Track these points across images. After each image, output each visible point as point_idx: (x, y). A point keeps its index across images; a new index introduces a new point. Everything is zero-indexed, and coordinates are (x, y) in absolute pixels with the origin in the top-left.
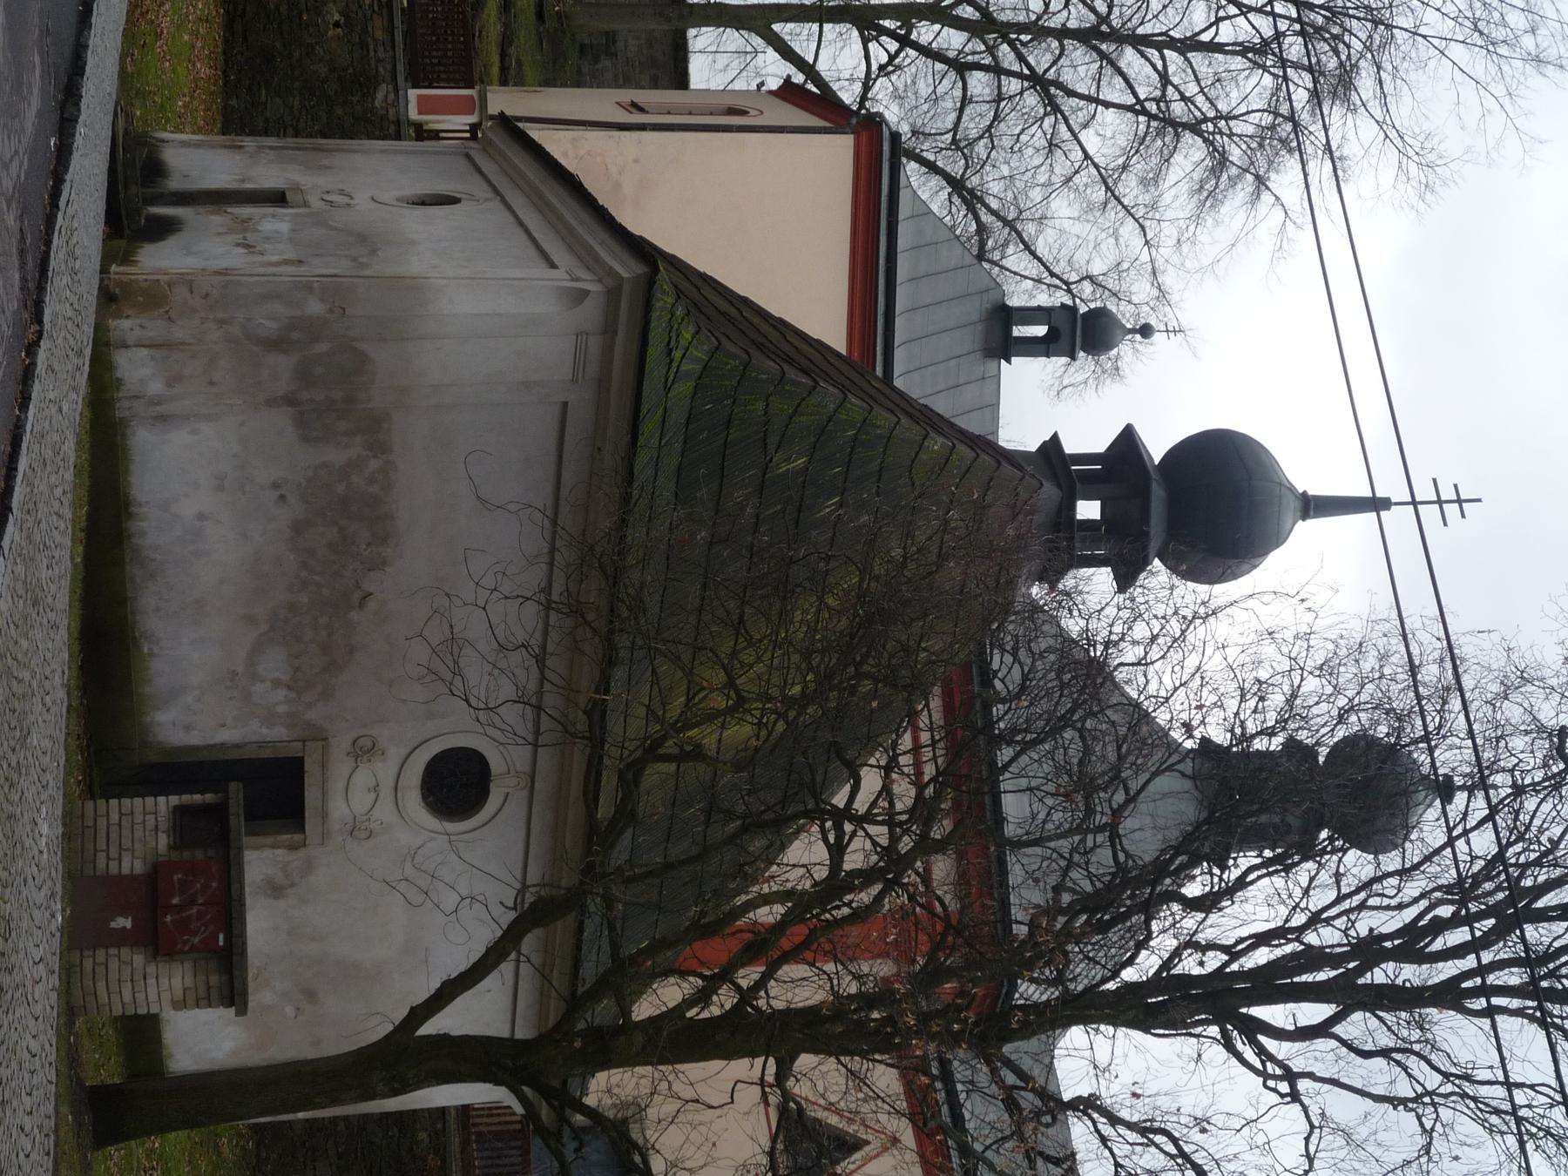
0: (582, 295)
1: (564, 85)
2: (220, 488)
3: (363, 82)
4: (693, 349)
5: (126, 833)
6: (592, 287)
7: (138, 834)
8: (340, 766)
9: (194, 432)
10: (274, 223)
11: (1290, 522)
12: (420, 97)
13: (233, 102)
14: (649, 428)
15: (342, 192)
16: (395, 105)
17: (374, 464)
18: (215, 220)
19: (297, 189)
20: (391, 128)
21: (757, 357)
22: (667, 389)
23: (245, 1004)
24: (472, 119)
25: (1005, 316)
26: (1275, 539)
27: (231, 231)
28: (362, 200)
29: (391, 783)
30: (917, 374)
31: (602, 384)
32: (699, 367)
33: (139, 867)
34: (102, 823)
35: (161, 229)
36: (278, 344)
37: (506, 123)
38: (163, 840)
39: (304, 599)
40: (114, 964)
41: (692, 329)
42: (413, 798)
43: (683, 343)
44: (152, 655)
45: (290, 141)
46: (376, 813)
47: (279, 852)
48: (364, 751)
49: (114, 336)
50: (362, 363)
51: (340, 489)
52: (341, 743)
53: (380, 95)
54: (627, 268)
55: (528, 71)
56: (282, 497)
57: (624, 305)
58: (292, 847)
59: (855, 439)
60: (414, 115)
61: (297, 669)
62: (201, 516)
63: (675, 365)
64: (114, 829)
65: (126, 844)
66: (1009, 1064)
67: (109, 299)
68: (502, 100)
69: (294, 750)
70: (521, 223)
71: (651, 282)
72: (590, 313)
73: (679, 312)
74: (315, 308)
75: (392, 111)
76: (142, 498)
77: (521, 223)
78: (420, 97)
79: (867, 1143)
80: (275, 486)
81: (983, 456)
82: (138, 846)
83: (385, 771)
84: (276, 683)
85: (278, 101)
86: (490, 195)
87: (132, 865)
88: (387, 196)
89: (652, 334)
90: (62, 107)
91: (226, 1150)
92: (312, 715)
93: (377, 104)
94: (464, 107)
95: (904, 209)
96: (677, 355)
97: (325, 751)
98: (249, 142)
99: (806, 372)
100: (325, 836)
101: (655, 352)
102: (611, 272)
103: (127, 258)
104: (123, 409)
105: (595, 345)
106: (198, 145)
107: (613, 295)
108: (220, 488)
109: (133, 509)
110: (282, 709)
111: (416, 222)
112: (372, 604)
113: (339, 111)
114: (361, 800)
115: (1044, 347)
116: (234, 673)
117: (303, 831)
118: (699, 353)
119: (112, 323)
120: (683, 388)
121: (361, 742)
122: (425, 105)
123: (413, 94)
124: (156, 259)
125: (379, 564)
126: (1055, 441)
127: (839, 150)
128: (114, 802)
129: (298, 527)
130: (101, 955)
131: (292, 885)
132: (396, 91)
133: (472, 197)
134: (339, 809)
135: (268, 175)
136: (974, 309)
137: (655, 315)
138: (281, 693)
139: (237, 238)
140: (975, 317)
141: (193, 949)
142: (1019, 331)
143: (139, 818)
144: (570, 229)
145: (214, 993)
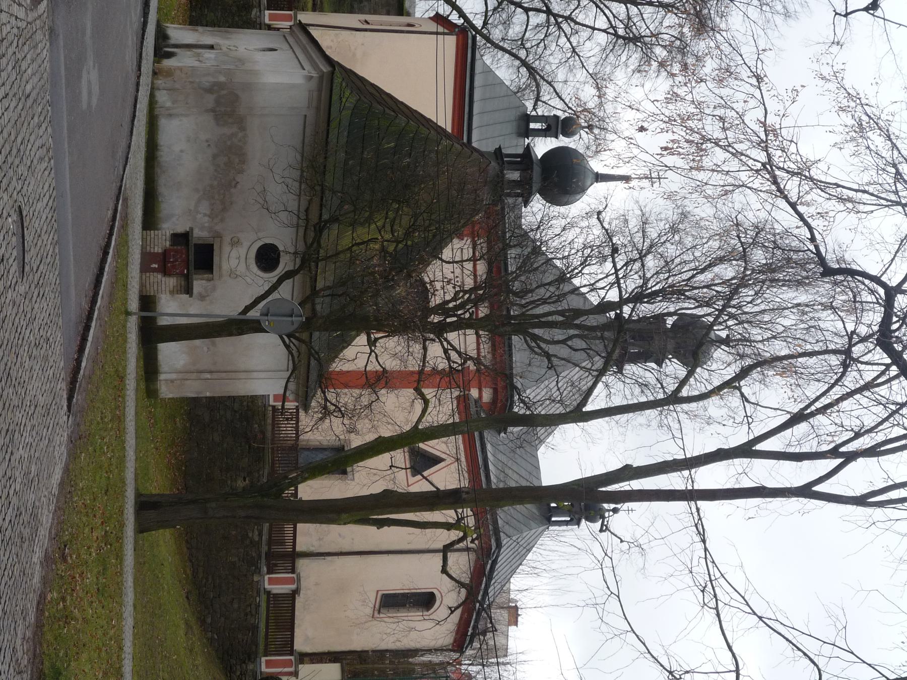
0: (312, 77)
1: (344, 12)
2: (188, 141)
3: (248, 8)
4: (350, 99)
5: (156, 241)
6: (314, 75)
7: (160, 241)
8: (226, 248)
9: (180, 120)
10: (209, 55)
11: (589, 183)
12: (270, 14)
13: (194, 14)
14: (334, 124)
15: (234, 46)
16: (260, 17)
17: (240, 135)
18: (188, 53)
19: (218, 45)
20: (256, 25)
21: (375, 104)
22: (340, 112)
23: (192, 293)
24: (291, 23)
25: (527, 118)
26: (583, 190)
27: (194, 56)
28: (241, 49)
29: (244, 256)
30: (484, 141)
31: (318, 109)
32: (352, 106)
33: (160, 251)
34: (149, 238)
35: (170, 55)
36: (209, 91)
37: (304, 28)
38: (168, 243)
39: (216, 183)
40: (152, 277)
41: (349, 91)
42: (254, 268)
43: (346, 96)
44: (162, 201)
45: (216, 29)
46: (239, 268)
47: (204, 282)
48: (235, 243)
49: (156, 86)
50: (237, 97)
51: (229, 143)
52: (227, 239)
53: (254, 13)
54: (325, 68)
55: (326, 5)
56: (209, 145)
57: (324, 84)
58: (209, 280)
59: (413, 138)
60: (267, 21)
61: (212, 210)
62: (182, 151)
63: (343, 104)
64: (152, 240)
65: (156, 243)
66: (446, 340)
67: (155, 73)
68: (305, 17)
69: (210, 241)
70: (297, 58)
71: (333, 73)
72: (314, 84)
73: (344, 84)
74: (222, 79)
75: (258, 20)
76: (162, 144)
77: (297, 58)
78: (270, 14)
79: (442, 460)
80: (207, 141)
81: (466, 149)
82: (160, 245)
83: (242, 251)
84: (205, 215)
85: (212, 14)
86: (289, 48)
87: (158, 250)
88: (250, 48)
89: (334, 91)
90: (144, 10)
91: (178, 424)
92: (218, 228)
93: (252, 16)
94: (288, 18)
95: (478, 68)
96: (344, 100)
97: (221, 242)
98: (200, 29)
99: (394, 111)
100: (221, 276)
101: (335, 97)
102: (321, 71)
103: (159, 62)
104: (157, 112)
105: (315, 94)
106: (181, 29)
107: (321, 78)
108: (188, 141)
109: (159, 148)
110: (206, 225)
111: (261, 57)
112: (239, 186)
113: (237, 19)
114: (233, 263)
115: (544, 133)
116: (190, 210)
117: (212, 273)
118: (353, 100)
119: (155, 82)
120: (347, 113)
121: (233, 240)
122: (272, 17)
123: (267, 12)
124: (167, 63)
125: (241, 171)
126: (500, 149)
127: (451, 41)
128: (152, 232)
129: (215, 157)
130: (148, 274)
131: (208, 296)
132: (260, 11)
133: (281, 49)
134: (225, 266)
135: (208, 40)
136: (513, 115)
137: (334, 85)
138: (206, 219)
139: (197, 59)
140: (513, 118)
141: (177, 274)
142: (533, 126)
143: (160, 236)
144: (311, 57)
145: (183, 290)
